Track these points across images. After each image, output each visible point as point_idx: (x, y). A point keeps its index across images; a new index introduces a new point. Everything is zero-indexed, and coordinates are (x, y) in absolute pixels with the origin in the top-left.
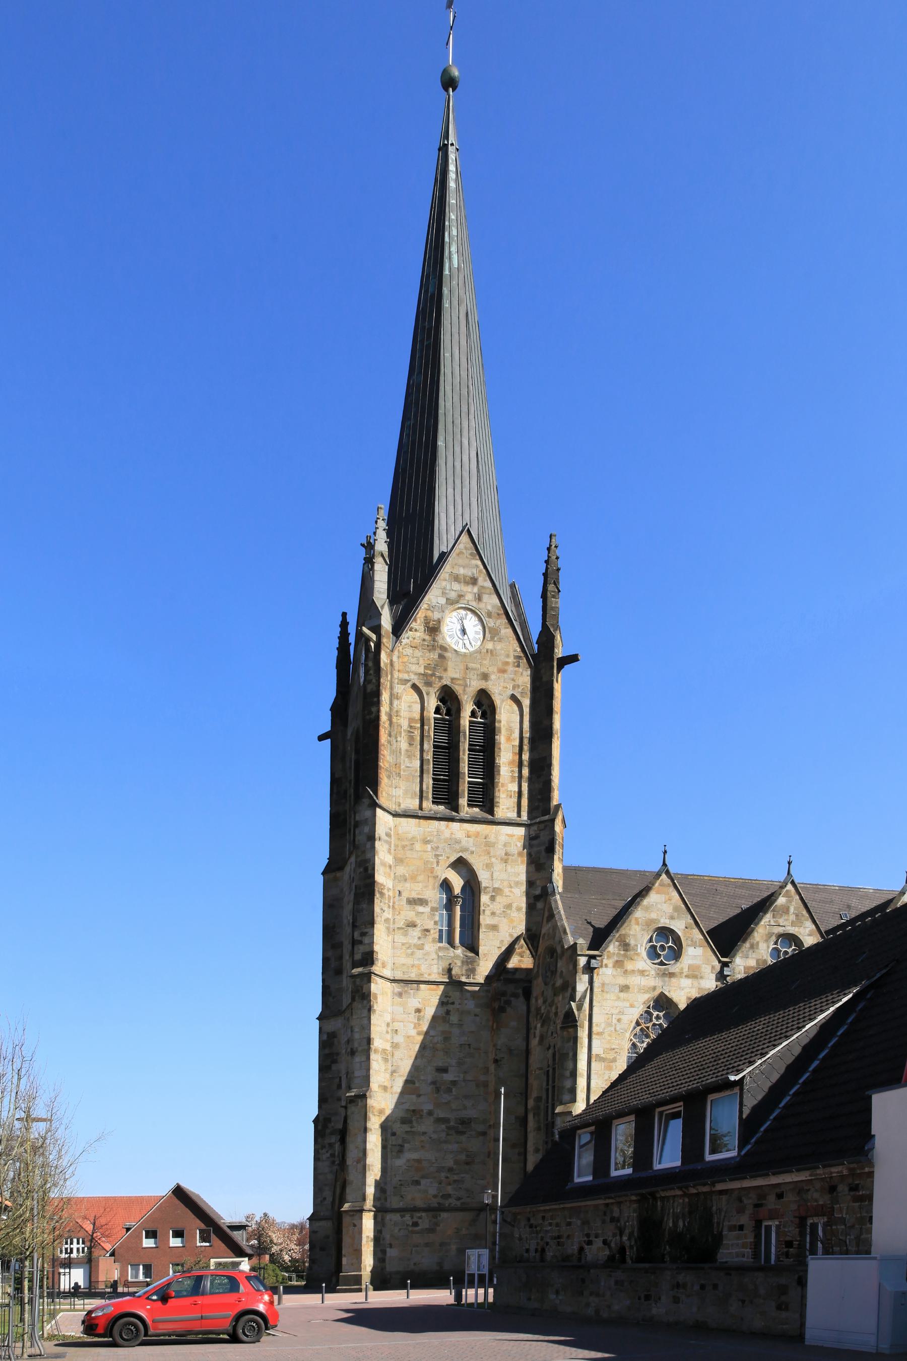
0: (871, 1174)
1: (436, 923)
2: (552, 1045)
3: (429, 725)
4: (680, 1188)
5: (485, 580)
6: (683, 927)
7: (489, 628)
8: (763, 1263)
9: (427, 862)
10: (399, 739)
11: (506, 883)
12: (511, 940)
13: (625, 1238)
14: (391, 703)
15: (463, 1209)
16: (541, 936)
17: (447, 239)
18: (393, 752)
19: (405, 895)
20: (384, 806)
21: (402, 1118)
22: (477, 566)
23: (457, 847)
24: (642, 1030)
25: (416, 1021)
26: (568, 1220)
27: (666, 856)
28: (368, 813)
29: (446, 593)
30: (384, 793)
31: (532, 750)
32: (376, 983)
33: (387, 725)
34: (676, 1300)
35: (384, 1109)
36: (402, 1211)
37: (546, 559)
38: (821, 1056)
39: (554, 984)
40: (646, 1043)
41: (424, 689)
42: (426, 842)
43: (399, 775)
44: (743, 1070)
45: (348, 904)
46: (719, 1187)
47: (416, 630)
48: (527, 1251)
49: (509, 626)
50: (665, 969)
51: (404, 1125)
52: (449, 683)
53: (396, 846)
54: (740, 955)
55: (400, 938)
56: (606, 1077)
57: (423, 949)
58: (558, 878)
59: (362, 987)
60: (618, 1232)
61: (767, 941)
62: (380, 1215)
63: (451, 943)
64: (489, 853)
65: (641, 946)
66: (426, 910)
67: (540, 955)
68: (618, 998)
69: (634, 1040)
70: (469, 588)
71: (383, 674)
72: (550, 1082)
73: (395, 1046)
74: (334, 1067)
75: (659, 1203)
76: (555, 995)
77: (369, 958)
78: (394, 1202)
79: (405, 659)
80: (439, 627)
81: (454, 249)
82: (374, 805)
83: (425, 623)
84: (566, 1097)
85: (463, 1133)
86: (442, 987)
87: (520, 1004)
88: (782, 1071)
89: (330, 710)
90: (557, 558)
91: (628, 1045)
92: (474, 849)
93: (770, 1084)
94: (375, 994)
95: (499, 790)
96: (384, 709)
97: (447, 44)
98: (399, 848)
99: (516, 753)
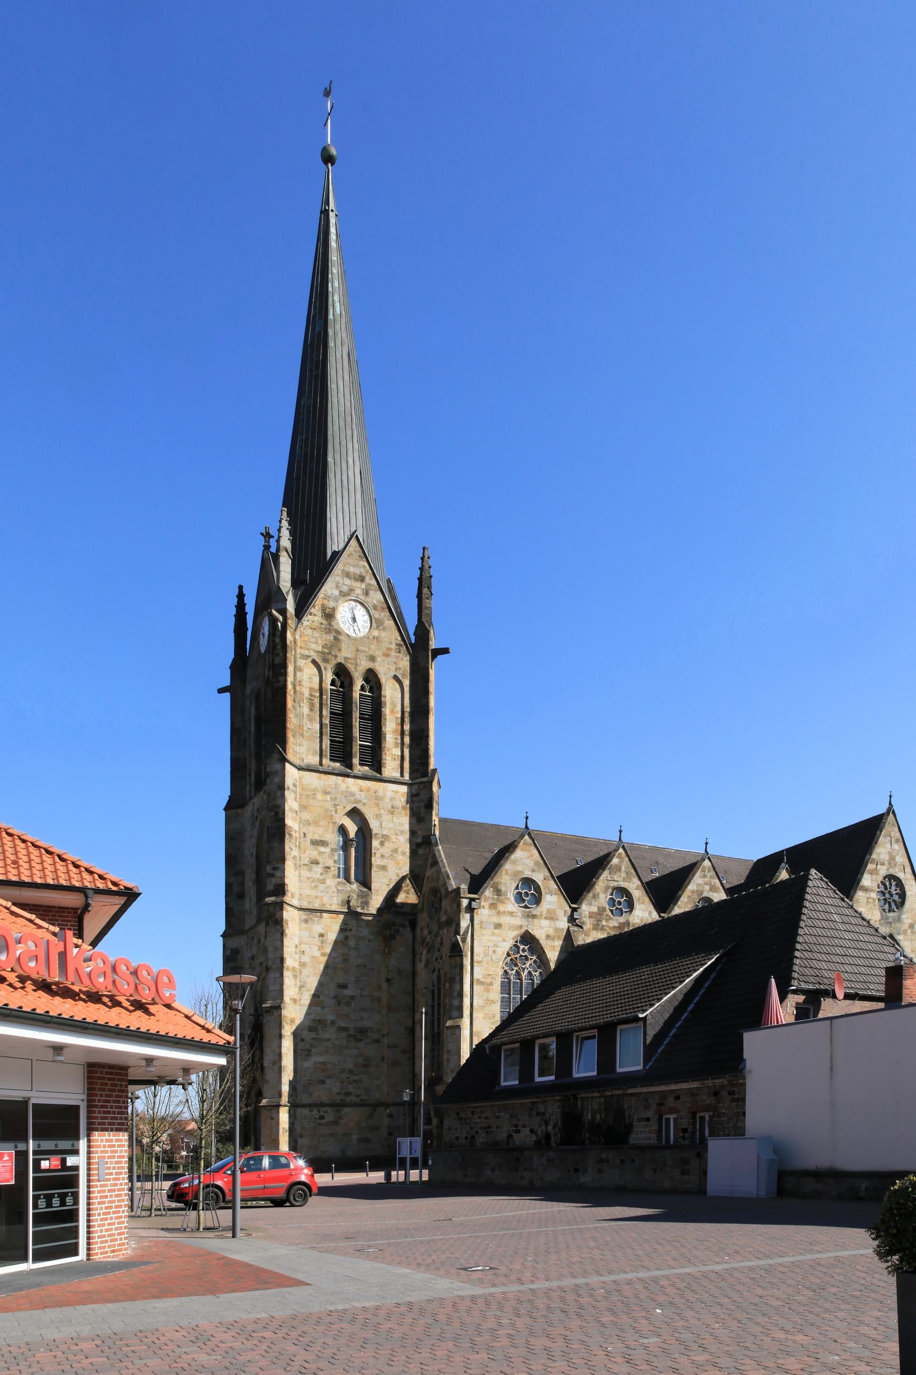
0: (744, 1084)
1: (335, 862)
2: (437, 969)
3: (327, 695)
4: (599, 1092)
5: (371, 579)
6: (543, 879)
7: (375, 618)
8: (664, 1143)
9: (327, 810)
10: (302, 705)
11: (392, 831)
12: (398, 879)
13: (550, 1128)
14: (295, 675)
15: (362, 1104)
16: (426, 878)
17: (330, 289)
18: (297, 715)
19: (309, 837)
20: (291, 760)
22: (364, 567)
23: (352, 798)
24: (511, 960)
25: (320, 944)
26: (497, 1114)
27: (528, 821)
28: (278, 766)
29: (339, 587)
30: (291, 750)
31: (412, 722)
32: (287, 911)
33: (292, 693)
34: (600, 1171)
35: (294, 1018)
36: (310, 1106)
37: (421, 566)
38: (695, 1001)
39: (439, 919)
40: (515, 971)
41: (322, 665)
42: (326, 793)
43: (302, 735)
44: (646, 1010)
45: (251, 838)
46: (630, 1091)
47: (315, 615)
48: (457, 1138)
49: (391, 618)
50: (529, 912)
51: (311, 1033)
52: (343, 661)
53: (301, 795)
54: (586, 903)
55: (305, 873)
56: (485, 998)
57: (324, 883)
59: (275, 914)
60: (544, 1123)
61: (605, 892)
62: (292, 1108)
64: (378, 805)
65: (510, 892)
67: (425, 894)
68: (493, 934)
69: (506, 968)
70: (358, 584)
71: (289, 650)
72: (436, 1000)
73: (303, 965)
75: (579, 1102)
76: (440, 928)
77: (281, 889)
78: (304, 1099)
79: (306, 638)
80: (334, 614)
81: (336, 298)
82: (284, 760)
83: (322, 610)
84: (455, 1013)
85: (360, 1040)
86: (342, 917)
87: (407, 933)
88: (671, 1011)
90: (430, 567)
91: (501, 972)
92: (366, 801)
93: (664, 1020)
94: (287, 920)
95: (385, 754)
96: (290, 679)
97: (325, 125)
98: (304, 797)
99: (398, 724)
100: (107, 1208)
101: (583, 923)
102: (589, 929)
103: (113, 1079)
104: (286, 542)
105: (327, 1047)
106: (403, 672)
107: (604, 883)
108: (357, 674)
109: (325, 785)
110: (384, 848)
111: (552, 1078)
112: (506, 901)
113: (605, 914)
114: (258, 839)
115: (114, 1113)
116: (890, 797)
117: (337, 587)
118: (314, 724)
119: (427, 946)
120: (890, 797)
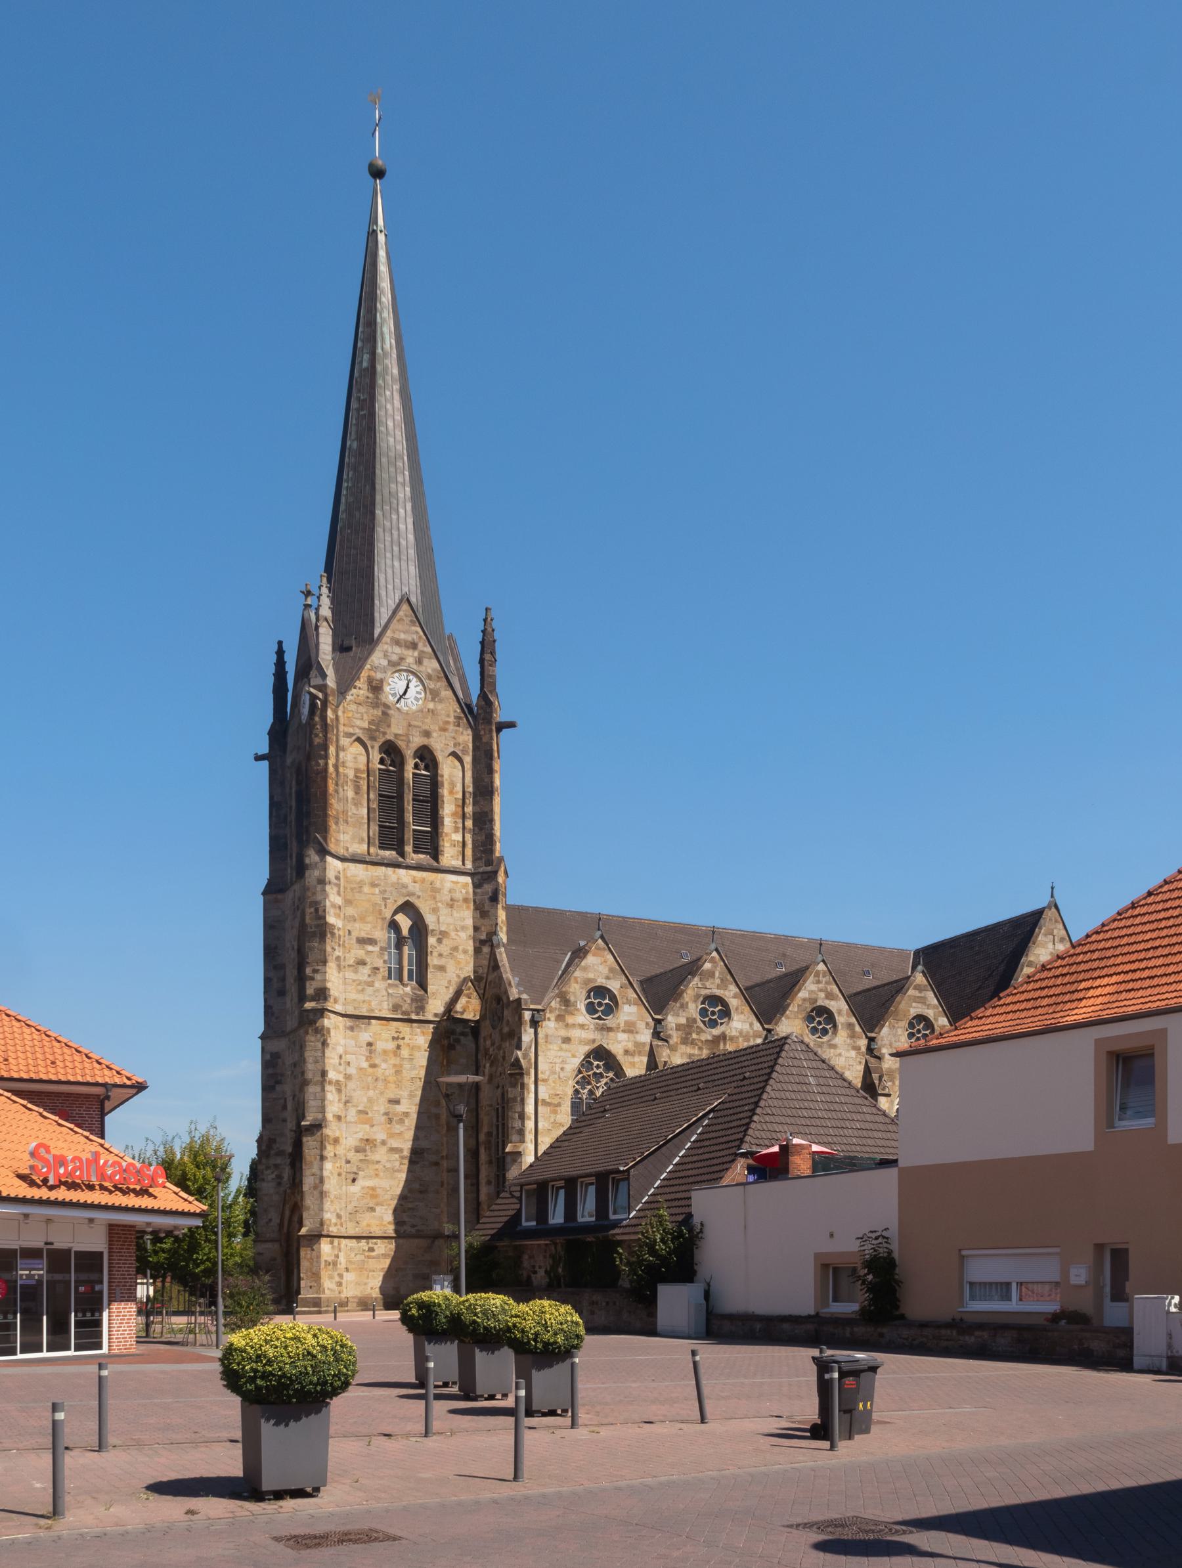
1: (385, 962)
2: (501, 1085)
3: (374, 776)
5: (425, 646)
6: (619, 986)
7: (430, 689)
10: (345, 788)
11: (451, 927)
17: (379, 320)
19: (355, 934)
20: (333, 851)
21: (356, 1147)
22: (417, 632)
23: (404, 891)
25: (368, 1054)
30: (332, 839)
32: (329, 1018)
33: (334, 776)
34: (592, 1313)
35: (338, 1138)
37: (483, 629)
39: (501, 1030)
41: (369, 743)
42: (373, 885)
45: (292, 928)
47: (360, 688)
50: (603, 1024)
51: (358, 1154)
52: (392, 738)
53: (345, 888)
55: (350, 975)
56: (552, 1120)
57: (373, 986)
58: (502, 925)
61: (695, 1001)
63: (401, 980)
64: (435, 898)
66: (376, 949)
68: (561, 1049)
69: (577, 1086)
70: (410, 652)
72: (500, 1119)
73: (348, 1077)
74: (278, 1088)
79: (350, 715)
82: (324, 852)
84: (515, 1137)
89: (269, 734)
90: (493, 630)
91: (570, 1092)
92: (420, 894)
95: (443, 840)
96: (332, 761)
98: (348, 890)
100: (121, 1319)
101: (670, 1036)
102: (677, 1043)
103: (126, 1234)
104: (326, 611)
105: (377, 1170)
106: (464, 747)
107: (694, 989)
108: (409, 752)
109: (372, 876)
110: (442, 946)
111: (534, 1223)
112: (576, 1012)
113: (695, 1025)
114: (299, 931)
115: (126, 1256)
116: (1052, 888)
117: (385, 656)
118: (360, 809)
119: (489, 1059)
120: (1052, 888)
